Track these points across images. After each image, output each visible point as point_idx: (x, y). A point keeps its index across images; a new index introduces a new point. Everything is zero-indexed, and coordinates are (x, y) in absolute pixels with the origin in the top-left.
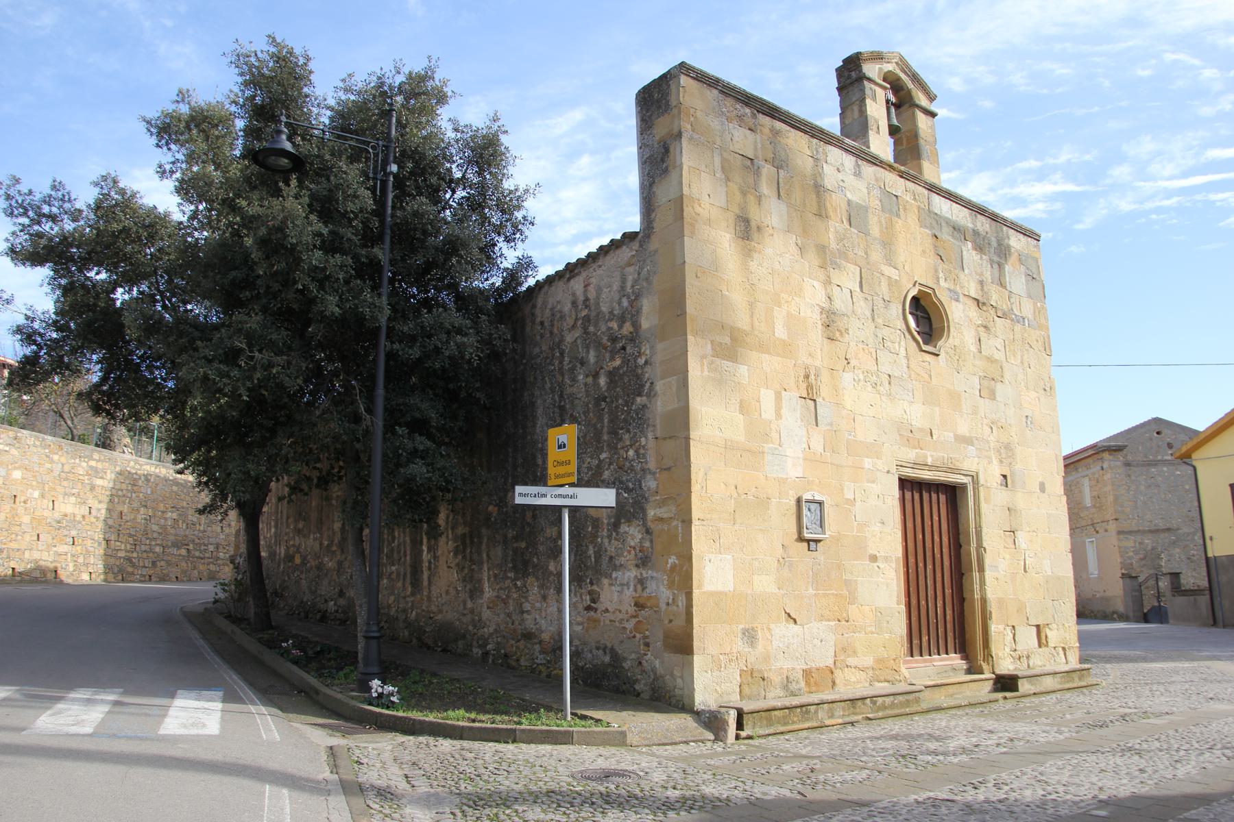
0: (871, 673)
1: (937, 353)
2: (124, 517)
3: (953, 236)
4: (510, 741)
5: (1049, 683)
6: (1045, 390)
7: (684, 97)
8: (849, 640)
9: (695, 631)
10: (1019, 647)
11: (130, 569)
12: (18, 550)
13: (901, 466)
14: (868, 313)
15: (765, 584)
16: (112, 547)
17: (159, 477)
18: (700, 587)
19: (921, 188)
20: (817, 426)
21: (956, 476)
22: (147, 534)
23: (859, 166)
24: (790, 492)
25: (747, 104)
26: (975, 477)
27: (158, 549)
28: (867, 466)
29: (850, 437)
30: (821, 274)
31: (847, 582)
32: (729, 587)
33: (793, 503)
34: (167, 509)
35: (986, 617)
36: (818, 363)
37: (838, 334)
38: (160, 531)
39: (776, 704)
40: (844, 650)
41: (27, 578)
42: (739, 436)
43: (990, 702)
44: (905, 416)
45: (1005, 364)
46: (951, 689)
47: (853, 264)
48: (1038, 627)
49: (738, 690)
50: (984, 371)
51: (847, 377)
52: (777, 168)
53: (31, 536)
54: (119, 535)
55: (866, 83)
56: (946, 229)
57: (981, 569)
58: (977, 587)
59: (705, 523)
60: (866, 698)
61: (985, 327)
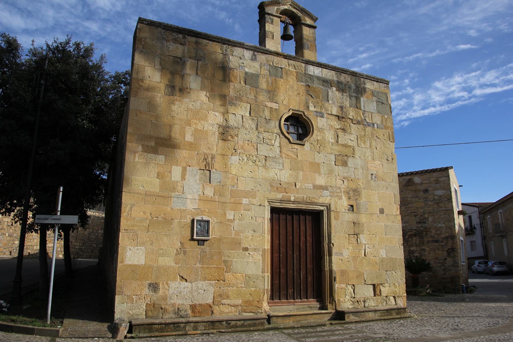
0: (240, 308)
1: (303, 144)
2: (79, 233)
3: (323, 85)
4: (10, 331)
5: (371, 315)
6: (388, 160)
7: (139, 33)
8: (225, 291)
9: (117, 283)
10: (358, 297)
11: (81, 253)
12: (31, 246)
13: (272, 202)
14: (254, 126)
16: (73, 244)
17: (95, 216)
18: (122, 262)
19: (300, 63)
20: (210, 183)
21: (314, 206)
22: (89, 239)
23: (255, 55)
24: (188, 216)
25: (180, 33)
26: (328, 207)
27: (94, 245)
28: (244, 202)
30: (222, 109)
31: (225, 262)
32: (143, 263)
33: (189, 221)
34: (99, 229)
35: (332, 280)
36: (214, 152)
37: (230, 138)
38: (95, 238)
39: (155, 321)
40: (221, 295)
41: (34, 256)
42: (156, 189)
43: (318, 326)
44: (276, 176)
45: (356, 148)
46: (298, 318)
47: (246, 103)
48: (374, 285)
49: (145, 313)
50: (339, 152)
51: (235, 159)
52: (198, 61)
53: (37, 240)
54: (76, 239)
55: (266, 16)
56: (316, 81)
57: (330, 255)
58: (327, 264)
59: (128, 231)
61: (343, 129)
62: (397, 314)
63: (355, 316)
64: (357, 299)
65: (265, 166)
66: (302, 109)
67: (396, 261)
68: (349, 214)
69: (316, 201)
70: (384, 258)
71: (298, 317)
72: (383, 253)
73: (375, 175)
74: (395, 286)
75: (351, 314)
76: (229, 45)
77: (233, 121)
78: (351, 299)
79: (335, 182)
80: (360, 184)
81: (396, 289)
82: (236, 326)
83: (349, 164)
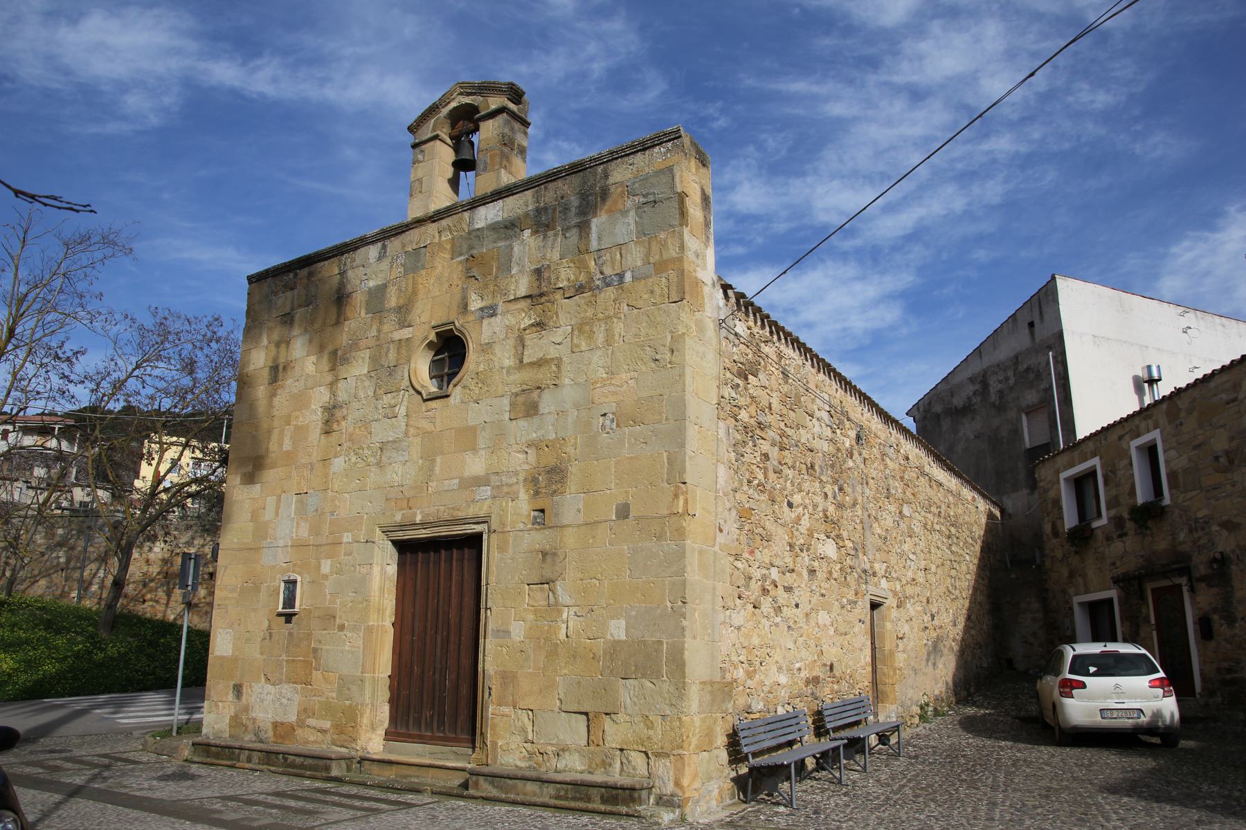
15: (254, 652)
29: (333, 517)
31: (315, 650)
60: (279, 753)
62: (604, 801)
63: (492, 783)
64: (539, 747)
65: (379, 464)
69: (461, 514)
70: (619, 641)
72: (618, 630)
73: (613, 414)
74: (648, 722)
75: (481, 779)
76: (348, 252)
78: (525, 745)
80: (568, 450)
81: (651, 732)
82: (293, 765)
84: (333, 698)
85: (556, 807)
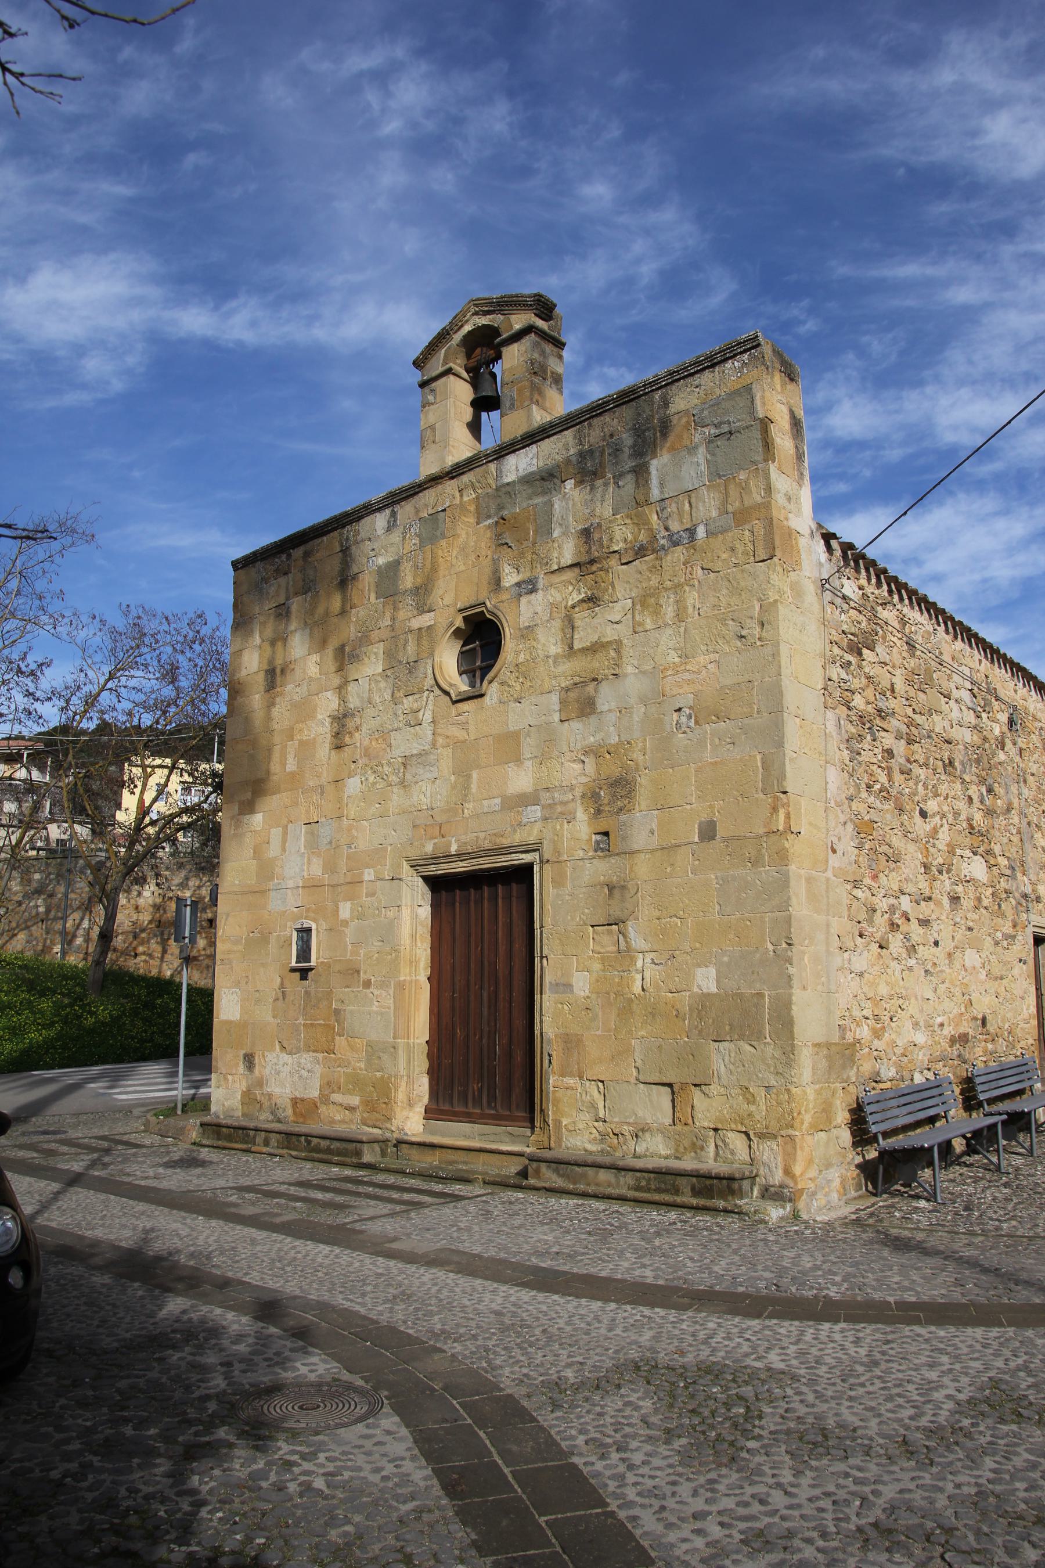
15: (265, 1015)
46: (451, 1156)
60: (301, 1135)
62: (696, 1192)
63: (556, 1171)
66: (483, 596)
67: (756, 1006)
68: (595, 861)
69: (506, 842)
70: (709, 994)
71: (450, 1151)
72: (706, 980)
73: (690, 708)
75: (543, 1166)
77: (354, 701)
78: (596, 1124)
79: (559, 774)
80: (635, 756)
82: (317, 1149)
83: (602, 705)
84: (361, 1069)
85: (636, 1201)
